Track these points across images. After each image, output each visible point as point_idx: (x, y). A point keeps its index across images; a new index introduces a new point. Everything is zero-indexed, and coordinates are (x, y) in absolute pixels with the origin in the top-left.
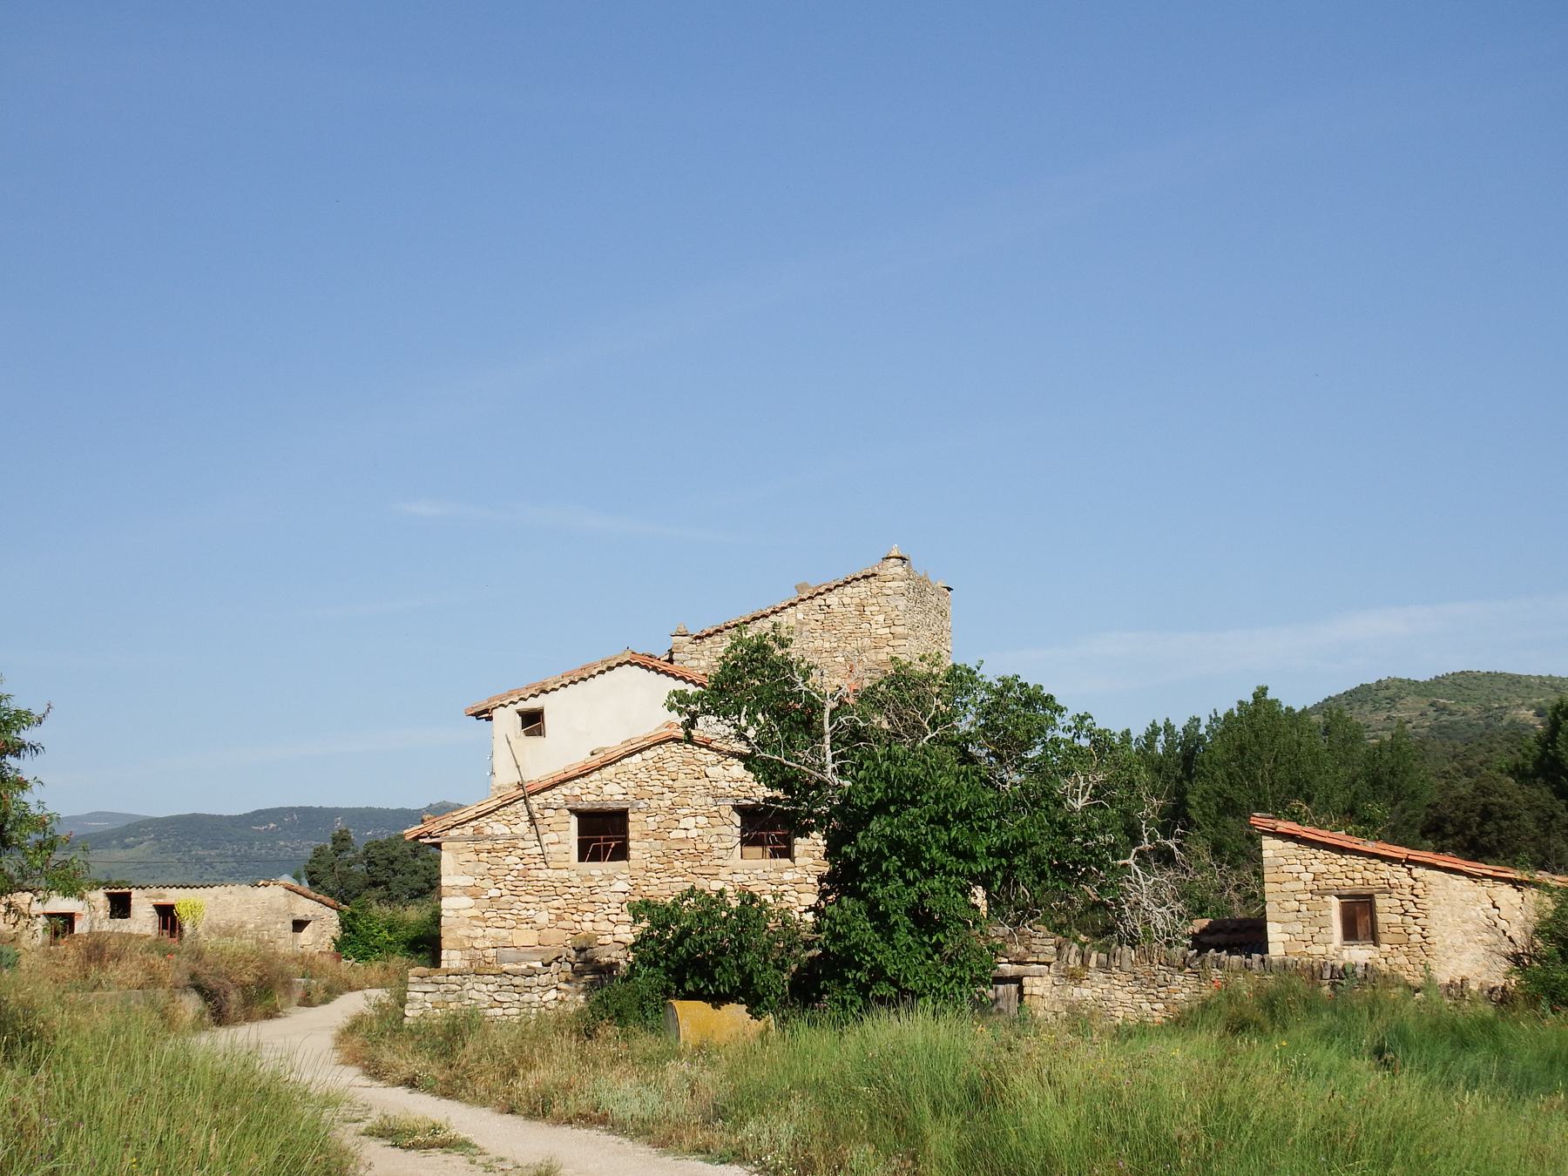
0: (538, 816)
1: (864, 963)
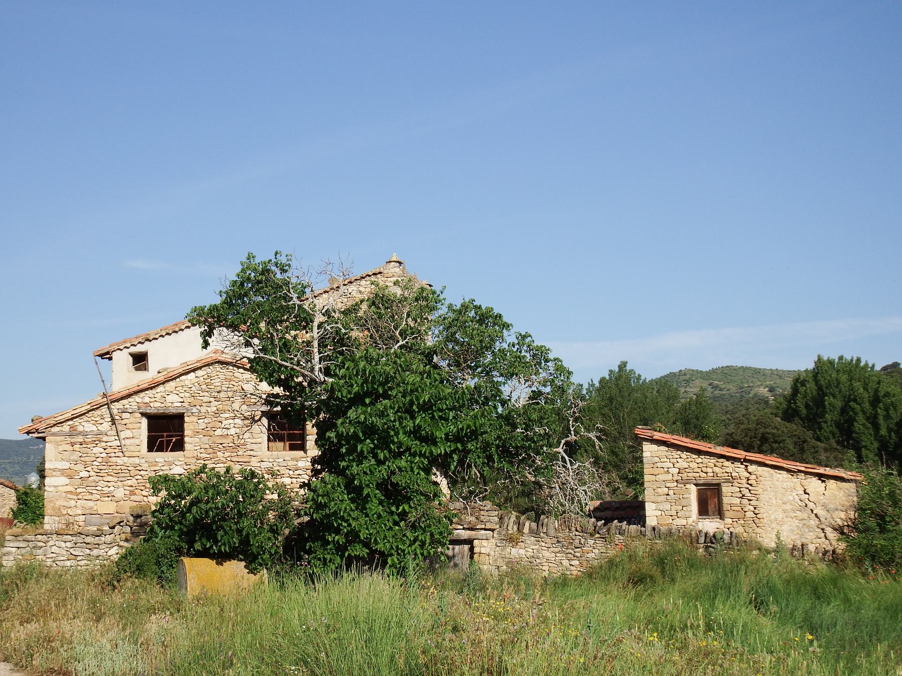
0: (117, 417)
1: (342, 528)
